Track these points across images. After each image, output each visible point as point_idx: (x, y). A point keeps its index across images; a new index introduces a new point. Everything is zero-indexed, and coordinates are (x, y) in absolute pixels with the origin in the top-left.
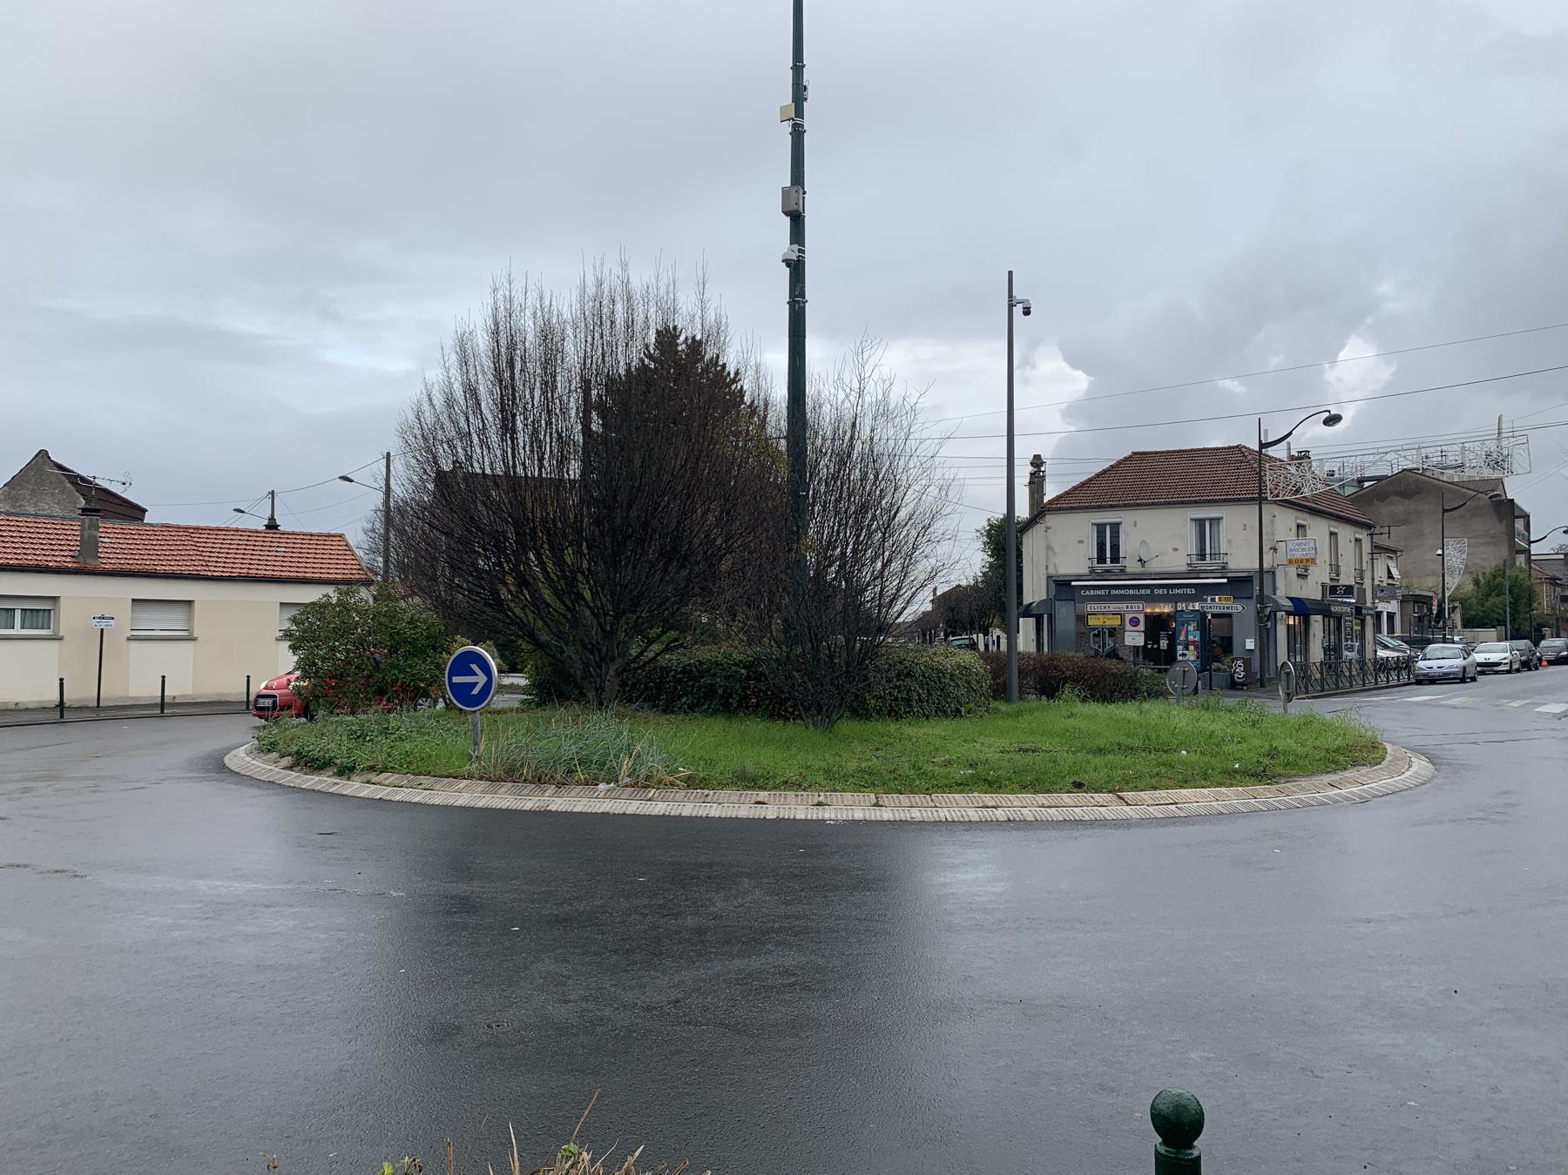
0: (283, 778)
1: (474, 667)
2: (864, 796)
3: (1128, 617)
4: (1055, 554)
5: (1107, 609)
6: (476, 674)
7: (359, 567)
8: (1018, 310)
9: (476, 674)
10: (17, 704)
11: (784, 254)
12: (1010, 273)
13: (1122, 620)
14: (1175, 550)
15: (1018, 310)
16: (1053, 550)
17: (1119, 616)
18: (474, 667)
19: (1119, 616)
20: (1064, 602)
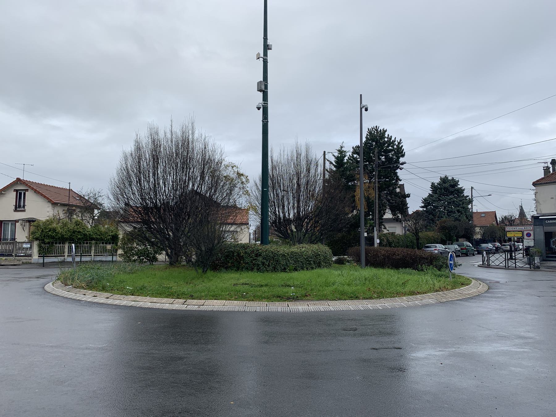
0: (62, 294)
2: (262, 303)
3: (525, 233)
4: (540, 204)
5: (516, 229)
8: (363, 109)
11: (257, 105)
12: (361, 95)
13: (523, 235)
15: (363, 109)
16: (539, 202)
17: (507, 233)
19: (507, 233)
20: (538, 226)
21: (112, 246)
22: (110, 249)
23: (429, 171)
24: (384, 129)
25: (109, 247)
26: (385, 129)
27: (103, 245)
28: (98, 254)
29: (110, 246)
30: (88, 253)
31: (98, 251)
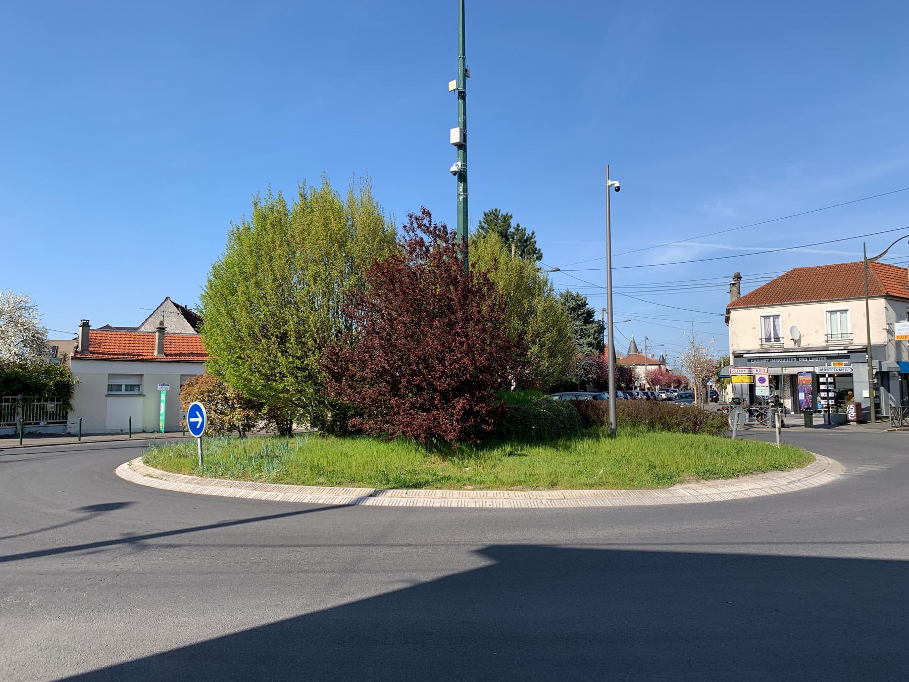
1: (197, 413)
6: (198, 417)
7: (886, 287)
9: (198, 417)
10: (122, 430)
12: (864, 243)
14: (817, 332)
18: (197, 413)
21: (57, 405)
22: (53, 412)
23: (592, 285)
24: (508, 213)
25: (52, 408)
26: (509, 215)
27: (39, 404)
28: (11, 423)
29: (53, 405)
30: (58, 419)
31: (25, 414)
